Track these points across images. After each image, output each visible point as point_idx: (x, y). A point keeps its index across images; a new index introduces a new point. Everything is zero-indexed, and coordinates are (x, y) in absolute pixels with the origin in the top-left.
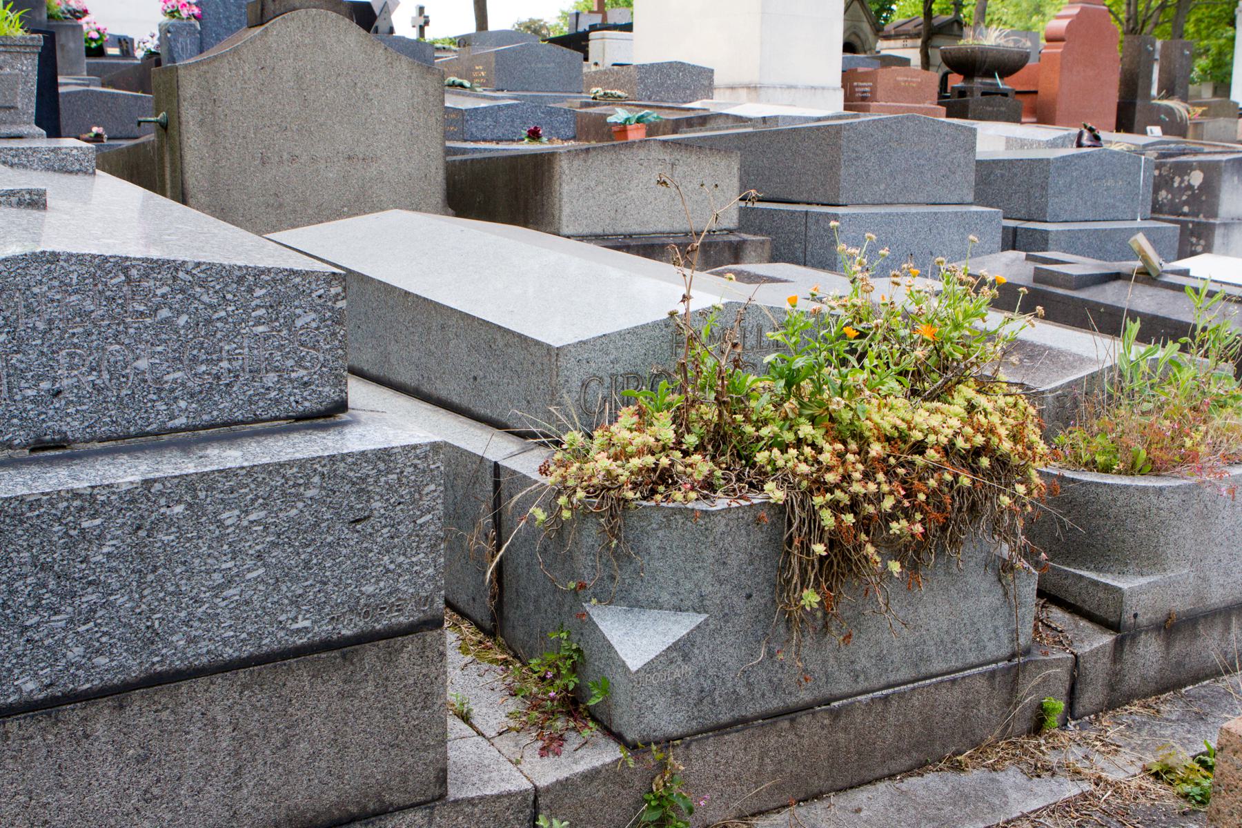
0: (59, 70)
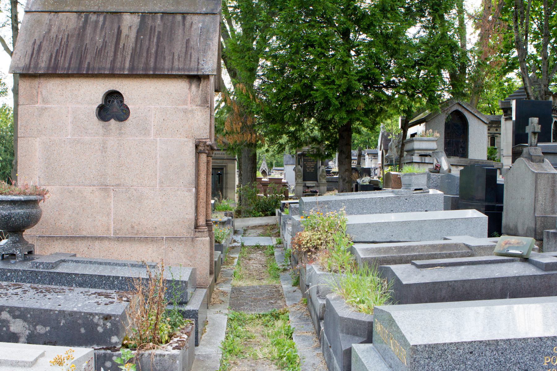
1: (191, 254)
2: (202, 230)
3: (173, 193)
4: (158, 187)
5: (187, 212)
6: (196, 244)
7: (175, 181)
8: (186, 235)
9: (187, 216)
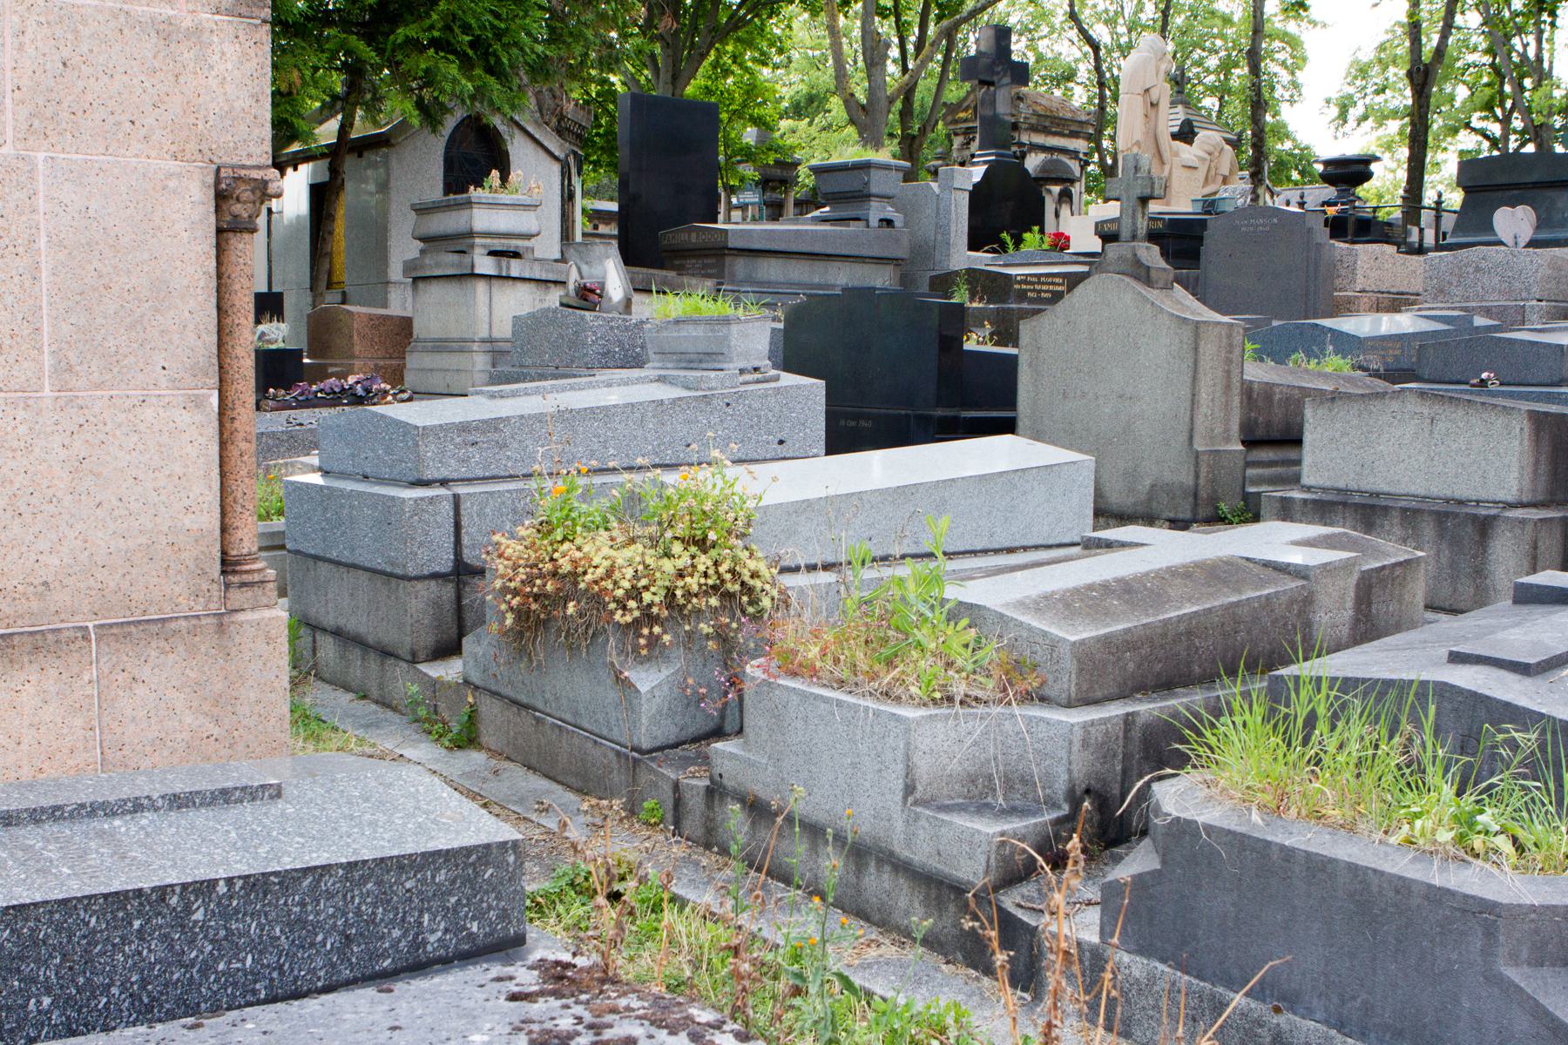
0: (782, 334)
1: (219, 686)
2: (257, 577)
3: (122, 417)
4: (47, 391)
5: (187, 503)
6: (237, 639)
7: (132, 359)
8: (185, 605)
9: (187, 521)
